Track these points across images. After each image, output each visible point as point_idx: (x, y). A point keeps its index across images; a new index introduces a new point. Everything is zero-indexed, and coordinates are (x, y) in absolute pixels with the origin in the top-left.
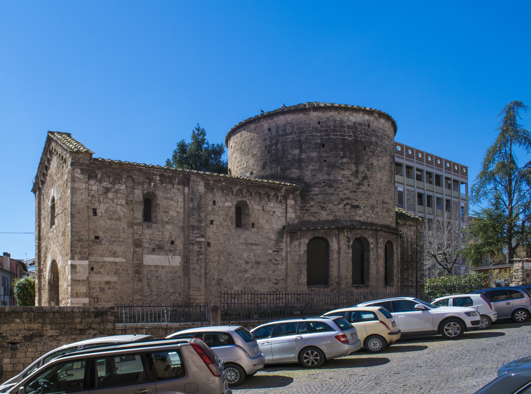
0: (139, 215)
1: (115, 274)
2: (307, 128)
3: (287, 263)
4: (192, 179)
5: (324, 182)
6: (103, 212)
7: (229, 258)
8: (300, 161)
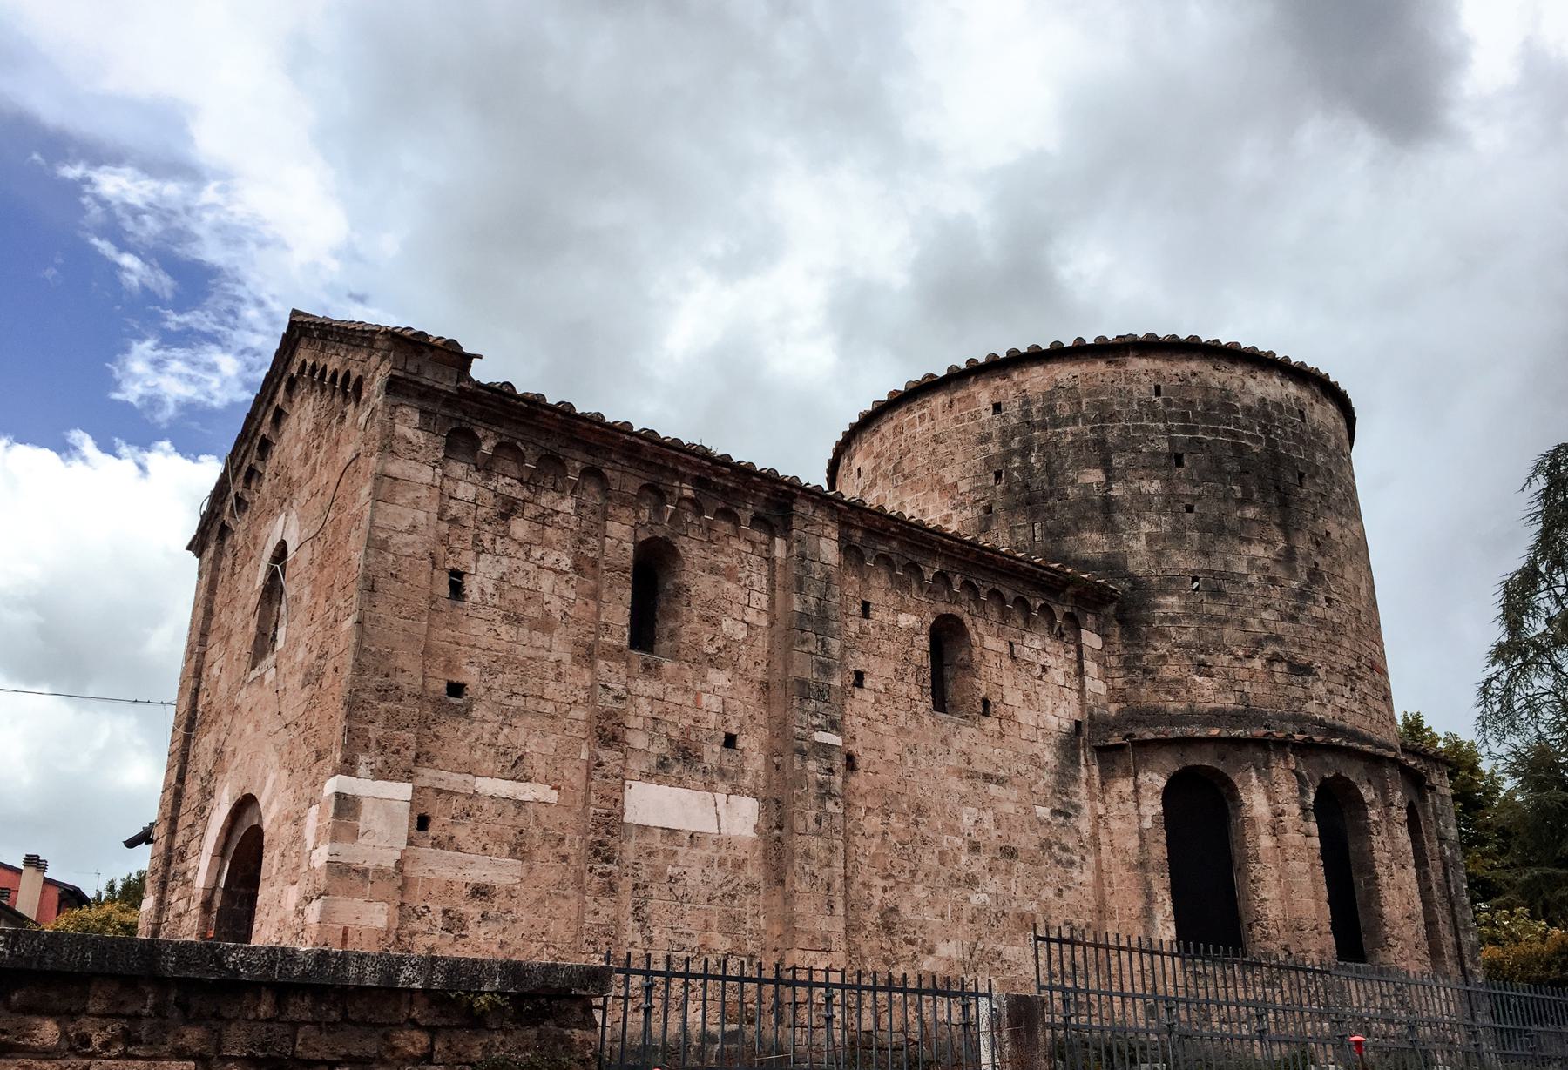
0: (618, 614)
1: (513, 852)
2: (1121, 404)
3: (1099, 863)
4: (801, 510)
5: (1195, 579)
6: (490, 589)
7: (916, 823)
8: (1108, 505)
